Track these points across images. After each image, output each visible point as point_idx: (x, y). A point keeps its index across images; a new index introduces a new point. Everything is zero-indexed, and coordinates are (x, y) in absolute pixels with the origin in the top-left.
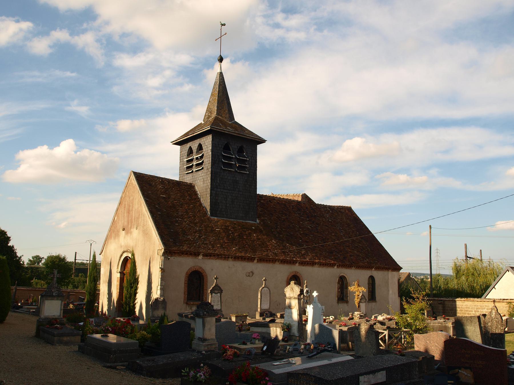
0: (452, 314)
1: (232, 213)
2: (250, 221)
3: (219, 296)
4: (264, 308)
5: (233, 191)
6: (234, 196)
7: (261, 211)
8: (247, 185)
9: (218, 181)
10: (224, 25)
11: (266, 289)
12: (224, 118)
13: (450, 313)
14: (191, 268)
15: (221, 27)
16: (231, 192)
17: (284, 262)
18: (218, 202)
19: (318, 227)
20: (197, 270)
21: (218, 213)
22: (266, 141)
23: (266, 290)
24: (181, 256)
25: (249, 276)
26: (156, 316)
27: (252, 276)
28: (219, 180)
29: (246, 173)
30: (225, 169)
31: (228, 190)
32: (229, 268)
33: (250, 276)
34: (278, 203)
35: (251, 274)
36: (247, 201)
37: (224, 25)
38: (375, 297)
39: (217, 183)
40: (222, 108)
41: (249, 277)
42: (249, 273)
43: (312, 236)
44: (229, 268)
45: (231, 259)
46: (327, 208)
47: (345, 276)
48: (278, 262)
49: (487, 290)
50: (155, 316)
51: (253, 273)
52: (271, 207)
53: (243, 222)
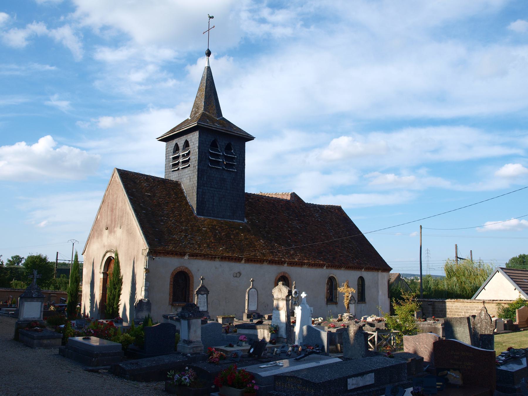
3: (206, 297)
6: (221, 194)
7: (249, 210)
10: (212, 17)
14: (176, 268)
15: (209, 19)
22: (255, 138)
24: (166, 256)
25: (236, 276)
26: (141, 318)
28: (206, 178)
31: (215, 188)
32: (216, 268)
35: (238, 275)
37: (212, 17)
41: (236, 278)
44: (216, 268)
45: (218, 259)
51: (240, 274)
53: (230, 221)
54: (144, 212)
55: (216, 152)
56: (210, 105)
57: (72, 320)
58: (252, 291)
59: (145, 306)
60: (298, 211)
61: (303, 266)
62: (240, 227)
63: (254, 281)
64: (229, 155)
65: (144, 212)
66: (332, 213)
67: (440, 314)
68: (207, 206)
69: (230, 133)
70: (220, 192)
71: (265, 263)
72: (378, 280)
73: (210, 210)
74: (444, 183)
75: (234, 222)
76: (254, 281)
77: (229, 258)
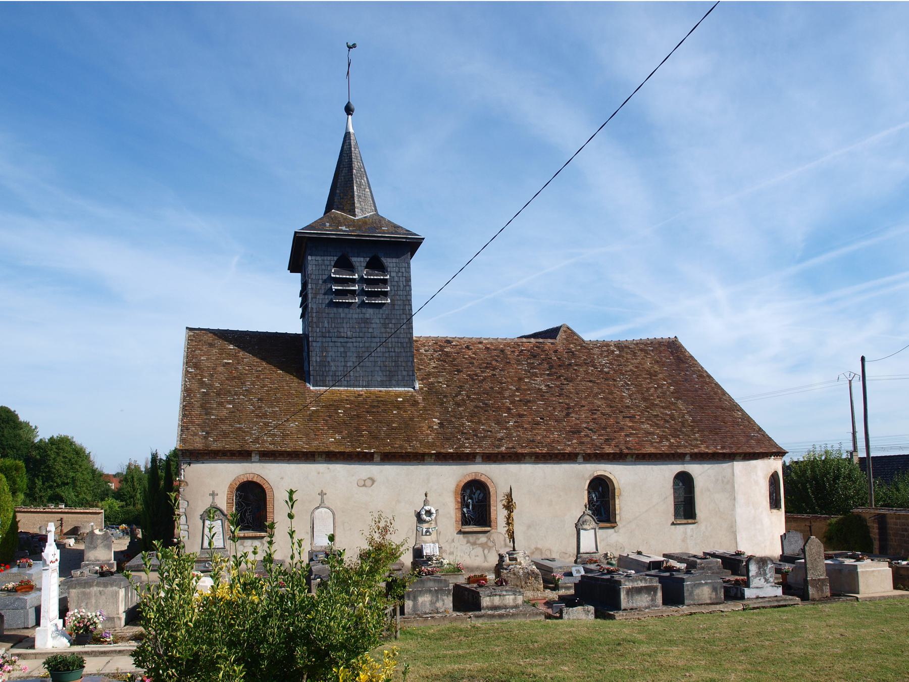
0: (896, 544)
1: (360, 376)
2: (395, 387)
3: (221, 524)
4: (322, 545)
5: (359, 337)
6: (361, 346)
7: (434, 368)
8: (390, 325)
9: (326, 325)
10: (354, 46)
11: (323, 511)
12: (348, 211)
13: (894, 540)
14: (238, 477)
15: (349, 51)
16: (354, 340)
17: (443, 458)
18: (328, 360)
19: (568, 384)
20: (250, 480)
21: (328, 379)
22: (423, 239)
23: (325, 512)
24: (216, 458)
25: (364, 485)
26: (93, 559)
27: (371, 486)
28: (328, 323)
29: (344, 302)
30: (337, 301)
31: (347, 338)
32: (319, 473)
33: (366, 486)
34: (487, 349)
35: (369, 483)
36: (391, 353)
37: (354, 46)
38: (695, 514)
39: (324, 329)
40: (346, 196)
41: (364, 488)
42: (365, 481)
43: (544, 404)
44: (319, 473)
45: (321, 458)
46: (609, 346)
47: (609, 476)
48: (632, 458)
49: (784, 484)
50: (90, 559)
51: (373, 481)
52: (464, 358)
53: (380, 391)
54: (203, 390)
55: (339, 278)
56: (345, 197)
57: (889, 597)
58: (321, 512)
59: (99, 541)
60: (558, 358)
61: (523, 460)
62: (399, 399)
63: (213, 492)
64: (372, 277)
65: (203, 390)
66: (645, 353)
67: (894, 540)
68: (333, 368)
69: (382, 239)
70: (359, 342)
71: (527, 458)
72: (733, 475)
73: (340, 375)
74: (304, 305)
75: (390, 391)
76: (213, 492)
77: (551, 456)
